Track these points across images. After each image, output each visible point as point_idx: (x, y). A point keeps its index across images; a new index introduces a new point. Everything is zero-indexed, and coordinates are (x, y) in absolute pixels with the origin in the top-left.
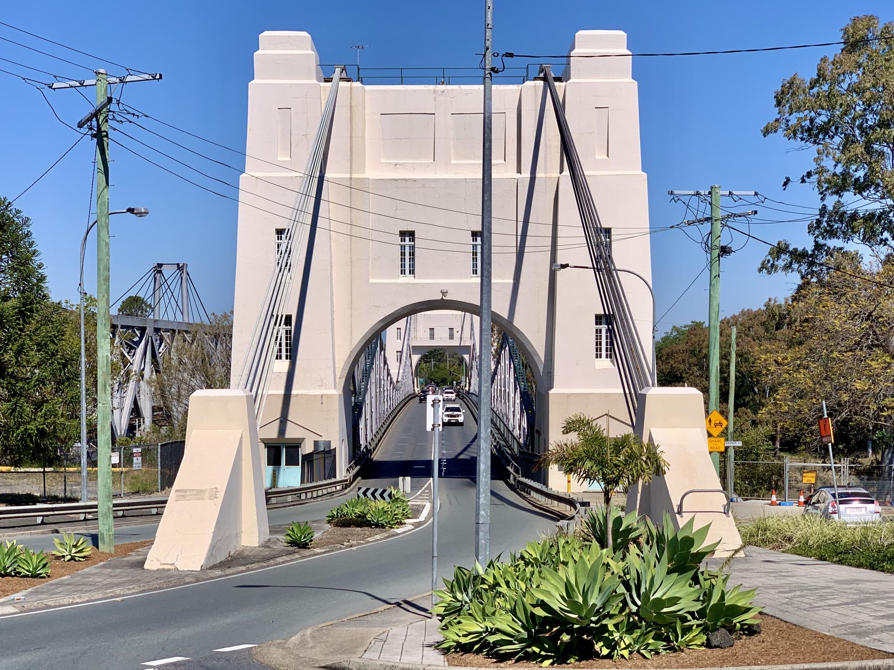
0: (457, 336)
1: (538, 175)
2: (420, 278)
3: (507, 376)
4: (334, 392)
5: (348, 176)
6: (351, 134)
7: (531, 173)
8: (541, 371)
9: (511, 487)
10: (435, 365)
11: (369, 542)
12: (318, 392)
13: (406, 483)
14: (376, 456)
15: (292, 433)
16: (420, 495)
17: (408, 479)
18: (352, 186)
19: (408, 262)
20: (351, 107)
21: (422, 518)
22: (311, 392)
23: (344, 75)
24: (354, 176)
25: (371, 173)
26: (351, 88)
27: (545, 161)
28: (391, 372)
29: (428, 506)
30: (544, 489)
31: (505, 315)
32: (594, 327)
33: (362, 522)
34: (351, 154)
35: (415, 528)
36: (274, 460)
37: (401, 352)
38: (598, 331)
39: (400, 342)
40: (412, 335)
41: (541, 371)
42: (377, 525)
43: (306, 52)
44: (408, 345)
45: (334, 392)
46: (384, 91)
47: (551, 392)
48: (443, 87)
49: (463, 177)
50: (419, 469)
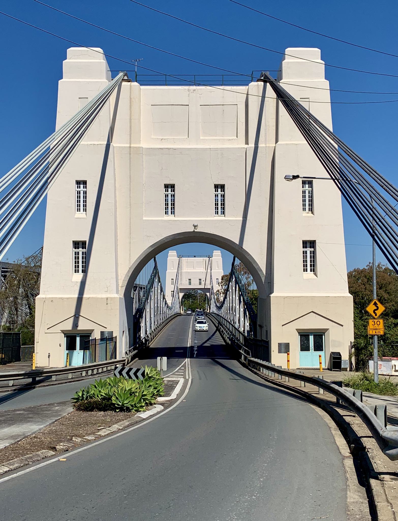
0: (203, 283)
1: (260, 145)
2: (178, 216)
3: (234, 296)
4: (116, 296)
5: (128, 145)
6: (131, 117)
7: (255, 144)
8: (263, 282)
9: (243, 365)
10: (192, 302)
11: (101, 437)
12: (104, 296)
13: (162, 362)
14: (152, 345)
15: (83, 325)
16: (177, 372)
17: (165, 359)
18: (132, 153)
19: (170, 207)
20: (131, 98)
21: (173, 396)
22: (99, 296)
23: (126, 78)
24: (132, 145)
25: (144, 145)
26: (131, 86)
27: (266, 135)
28: (167, 302)
29: (182, 381)
30: (269, 365)
31: (237, 241)
32: (302, 250)
33: (106, 405)
34: (130, 131)
35: (166, 408)
36: (71, 346)
37: (174, 291)
38: (305, 253)
39: (173, 286)
40: (179, 282)
41: (263, 282)
42: (122, 409)
43: (100, 61)
44: (177, 287)
45: (116, 296)
46: (154, 89)
47: (272, 295)
48: (194, 87)
49: (208, 147)
50: (175, 353)
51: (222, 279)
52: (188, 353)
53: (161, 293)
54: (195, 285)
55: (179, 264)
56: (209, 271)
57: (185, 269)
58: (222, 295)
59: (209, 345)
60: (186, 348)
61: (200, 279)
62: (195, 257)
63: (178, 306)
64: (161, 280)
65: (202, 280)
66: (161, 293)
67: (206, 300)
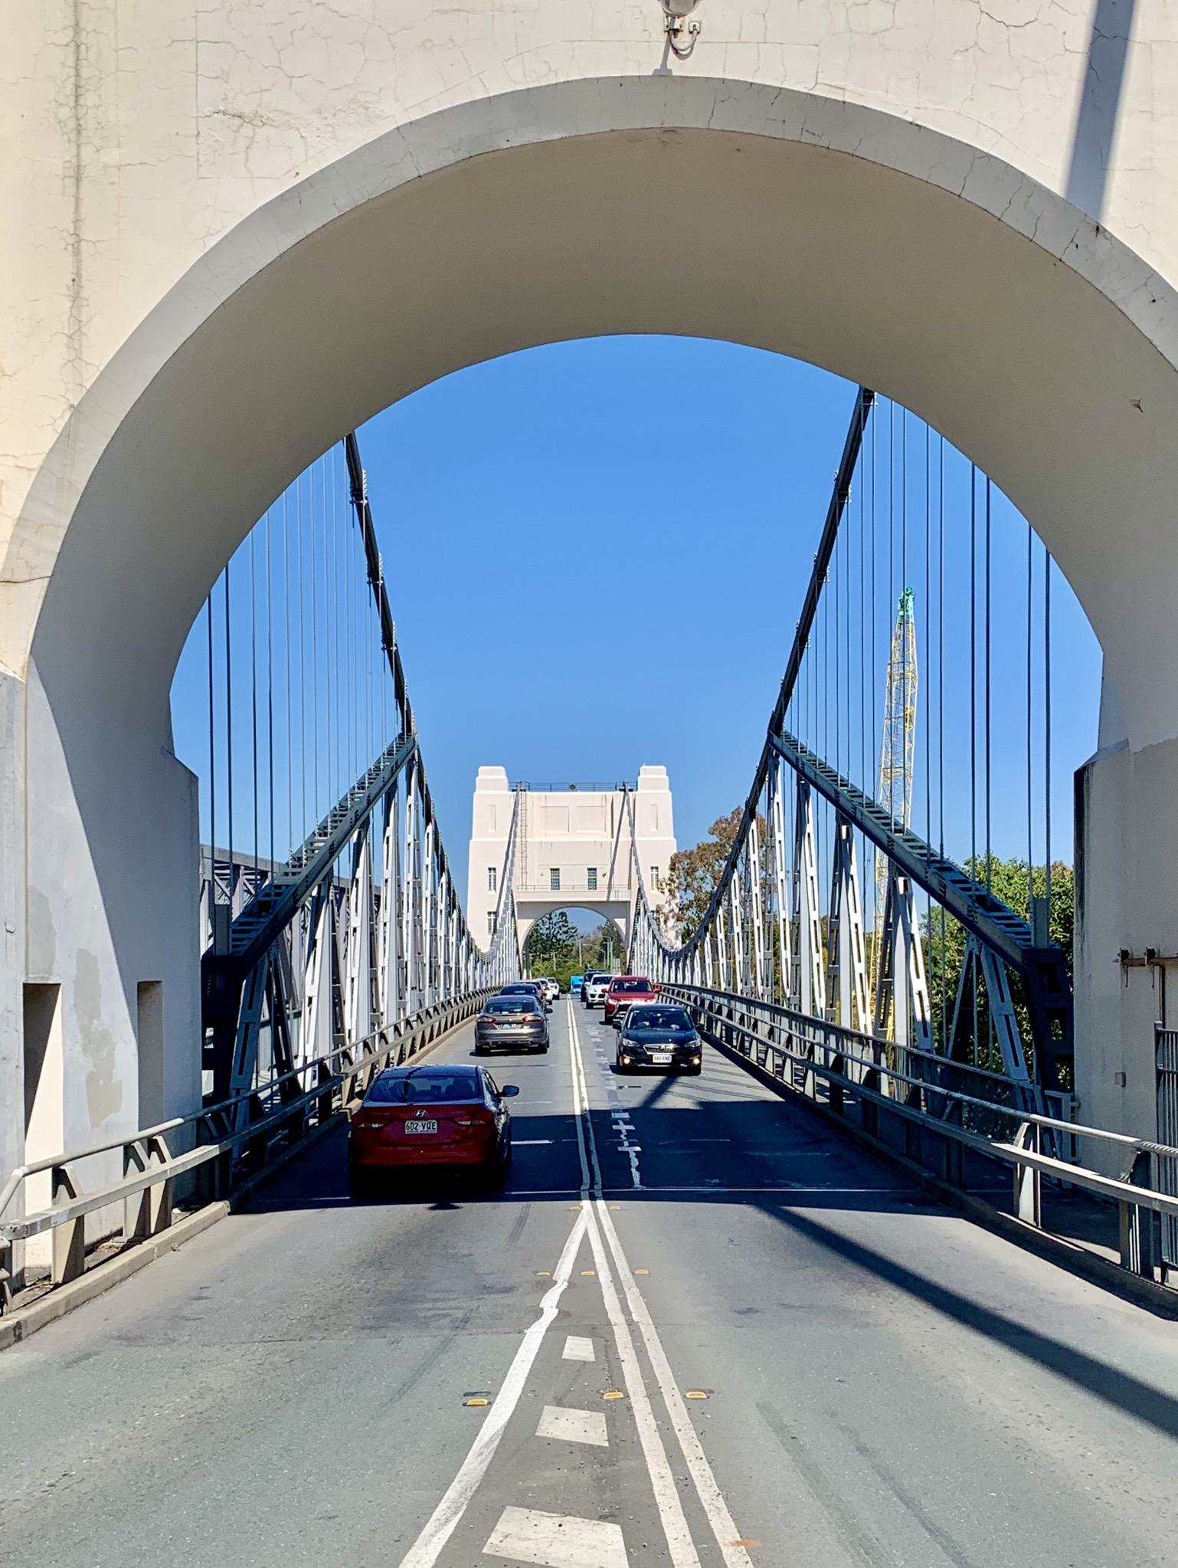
0: (602, 882)
31: (1048, 167)
40: (516, 882)
51: (673, 868)
52: (586, 1162)
53: (449, 914)
54: (575, 888)
55: (515, 814)
56: (625, 838)
57: (536, 833)
58: (671, 922)
59: (686, 1104)
60: (565, 1122)
61: (592, 870)
62: (573, 788)
63: (513, 963)
64: (448, 864)
65: (599, 873)
66: (449, 914)
67: (613, 943)
